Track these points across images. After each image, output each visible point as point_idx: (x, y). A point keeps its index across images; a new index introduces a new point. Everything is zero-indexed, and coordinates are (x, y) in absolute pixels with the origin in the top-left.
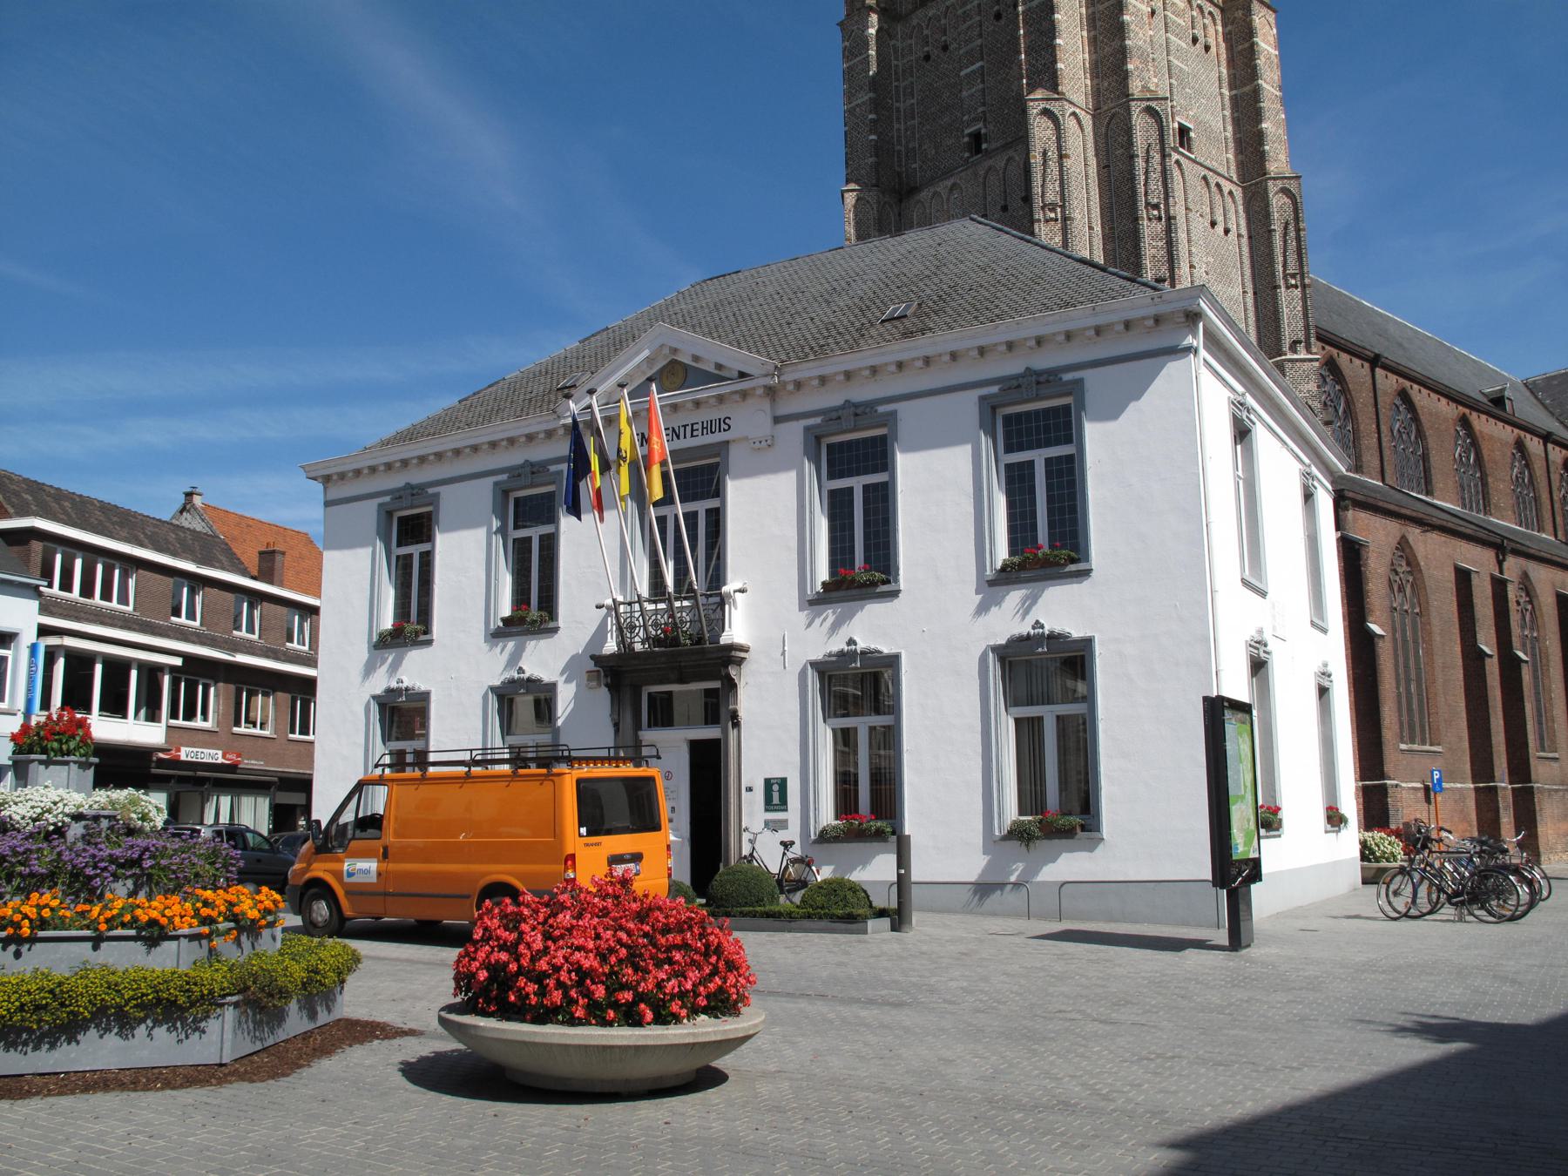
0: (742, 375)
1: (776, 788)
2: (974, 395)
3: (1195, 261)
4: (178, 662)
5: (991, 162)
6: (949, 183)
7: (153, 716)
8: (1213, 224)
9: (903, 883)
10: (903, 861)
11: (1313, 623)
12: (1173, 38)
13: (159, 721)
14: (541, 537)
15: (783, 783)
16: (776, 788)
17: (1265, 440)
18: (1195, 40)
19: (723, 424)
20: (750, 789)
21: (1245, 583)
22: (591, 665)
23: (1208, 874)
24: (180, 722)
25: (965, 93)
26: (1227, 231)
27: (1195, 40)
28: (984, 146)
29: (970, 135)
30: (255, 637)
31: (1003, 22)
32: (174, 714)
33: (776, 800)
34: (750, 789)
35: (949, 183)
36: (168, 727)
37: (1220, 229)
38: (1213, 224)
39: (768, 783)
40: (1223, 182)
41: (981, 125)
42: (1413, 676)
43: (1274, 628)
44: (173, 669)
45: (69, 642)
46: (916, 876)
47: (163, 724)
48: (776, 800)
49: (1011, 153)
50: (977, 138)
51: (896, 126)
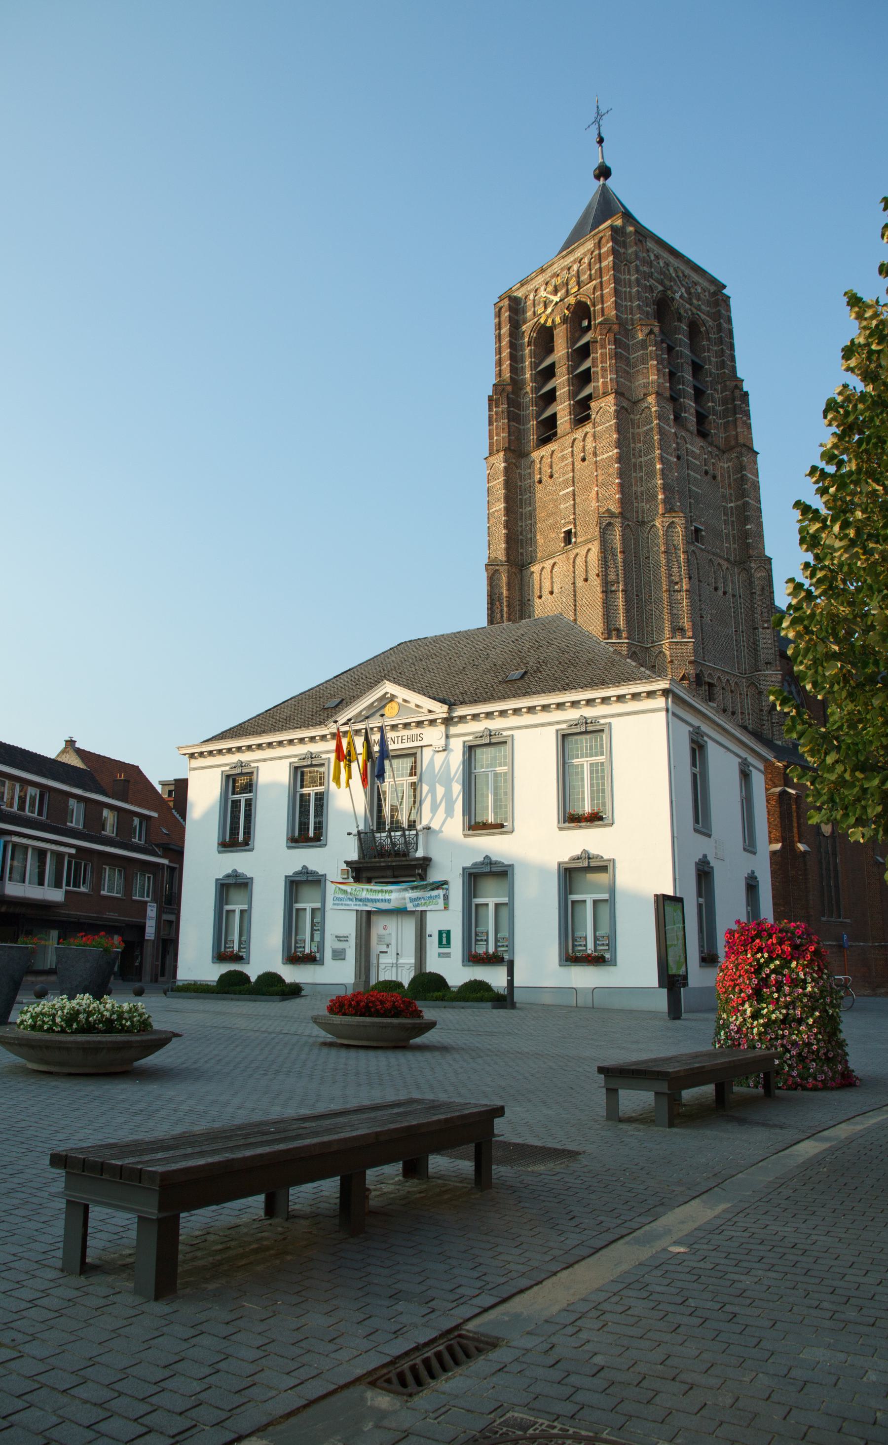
0: (430, 711)
1: (444, 935)
2: (553, 728)
3: (704, 613)
4: (73, 851)
5: (577, 551)
6: (552, 562)
7: (58, 884)
8: (716, 589)
9: (511, 982)
10: (511, 973)
11: (745, 849)
12: (692, 473)
13: (61, 887)
14: (316, 794)
15: (448, 933)
16: (444, 935)
17: (713, 751)
18: (706, 473)
19: (420, 737)
20: (430, 936)
21: (696, 830)
22: (344, 867)
23: (655, 983)
24: (71, 888)
25: (562, 506)
26: (725, 593)
27: (706, 473)
28: (573, 540)
29: (565, 532)
30: (44, 818)
31: (586, 463)
32: (68, 884)
33: (444, 942)
34: (430, 936)
35: (552, 562)
36: (67, 892)
37: (721, 593)
38: (716, 589)
39: (440, 933)
40: (721, 561)
41: (572, 526)
42: (832, 876)
43: (716, 854)
44: (70, 855)
45: (15, 839)
46: (516, 983)
47: (63, 890)
48: (444, 942)
49: (590, 546)
50: (568, 533)
51: (520, 524)
